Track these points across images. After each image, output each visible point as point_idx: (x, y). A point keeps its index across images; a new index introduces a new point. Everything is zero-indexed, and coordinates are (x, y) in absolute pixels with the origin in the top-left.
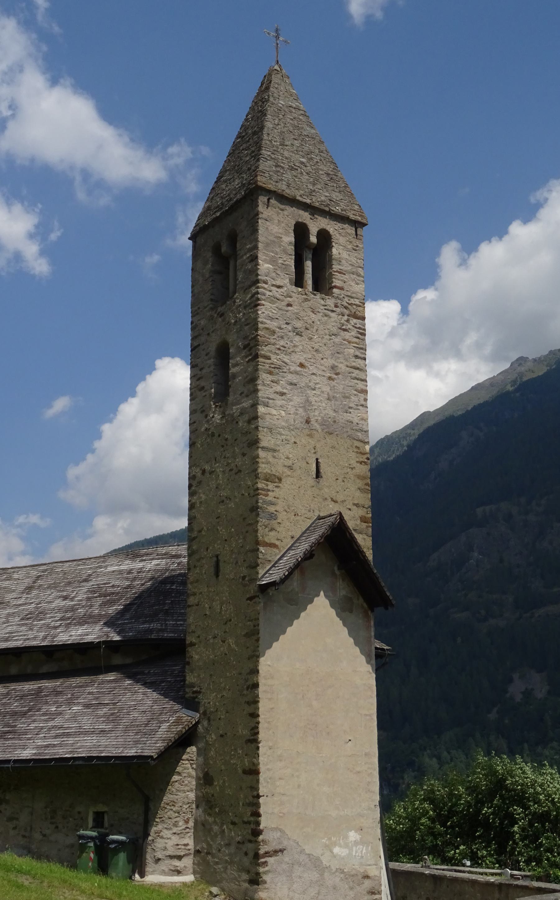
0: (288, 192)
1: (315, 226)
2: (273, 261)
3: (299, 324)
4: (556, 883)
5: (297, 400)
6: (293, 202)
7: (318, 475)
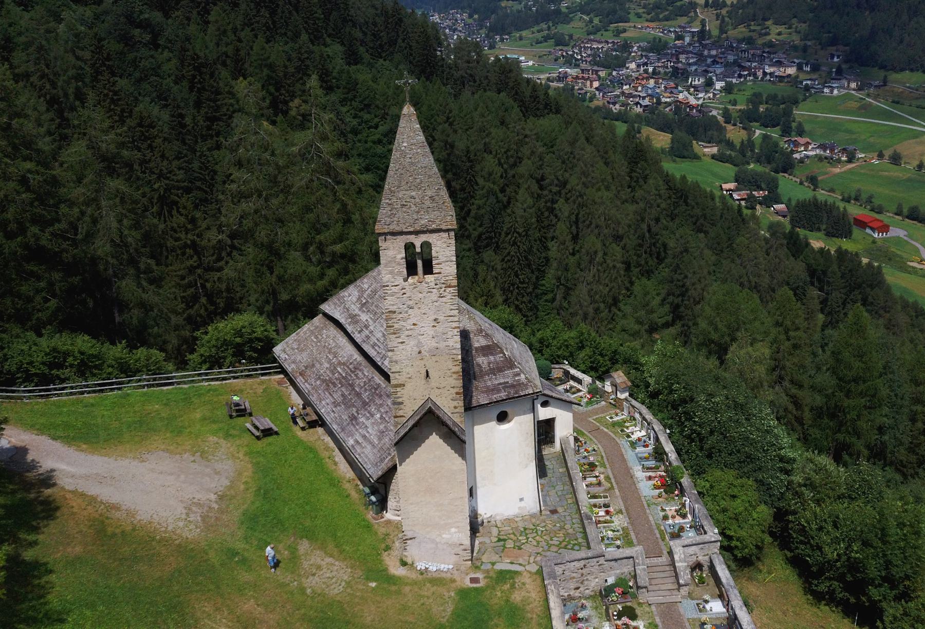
0: (398, 229)
1: (418, 241)
2: (391, 273)
3: (411, 303)
4: (912, 70)
5: (413, 343)
6: (401, 233)
7: (428, 376)
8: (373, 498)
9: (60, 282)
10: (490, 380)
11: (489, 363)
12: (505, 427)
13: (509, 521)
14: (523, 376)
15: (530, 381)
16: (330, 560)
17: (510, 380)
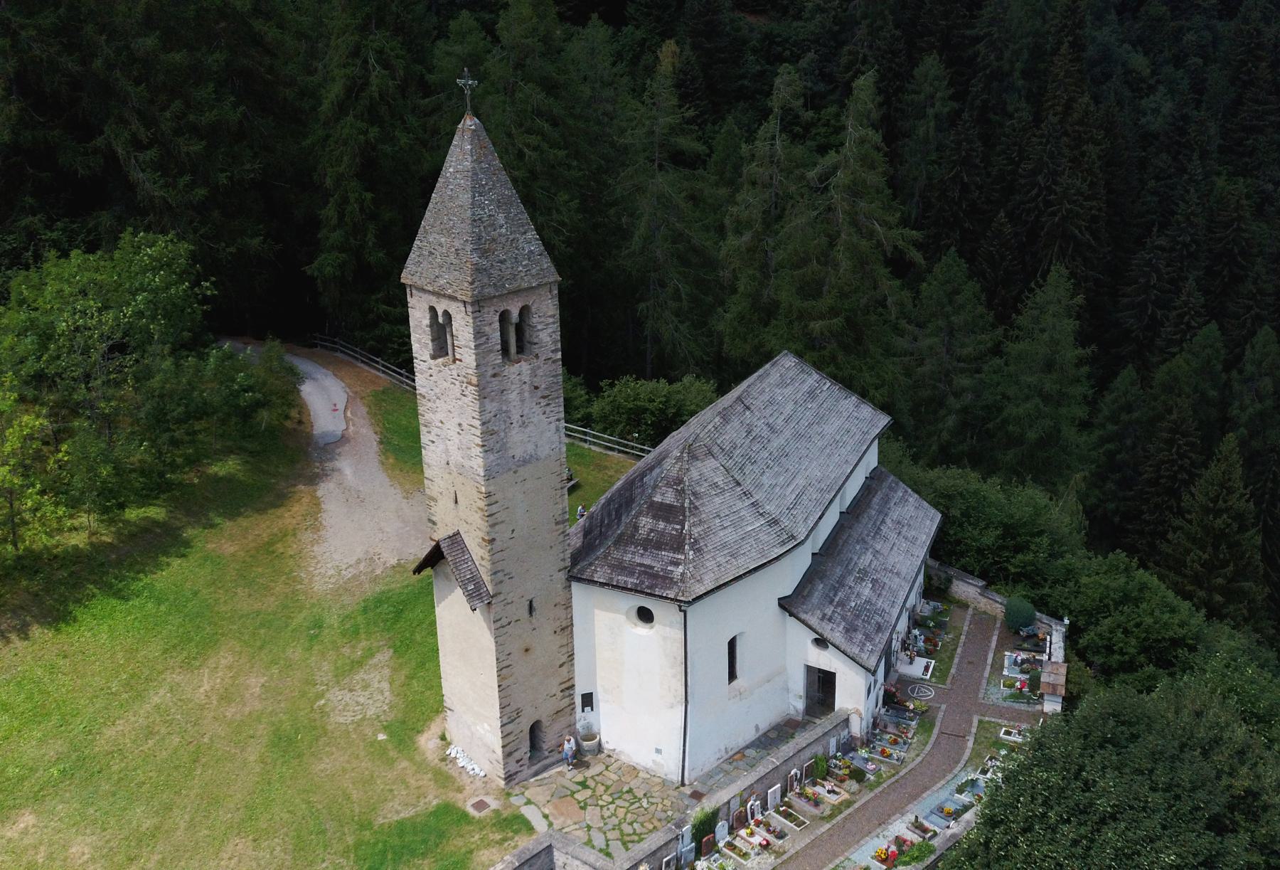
8: (105, 471)
9: (111, 443)
10: (633, 553)
11: (652, 531)
12: (642, 630)
13: (634, 770)
14: (681, 569)
15: (682, 581)
16: (385, 685)
17: (658, 566)
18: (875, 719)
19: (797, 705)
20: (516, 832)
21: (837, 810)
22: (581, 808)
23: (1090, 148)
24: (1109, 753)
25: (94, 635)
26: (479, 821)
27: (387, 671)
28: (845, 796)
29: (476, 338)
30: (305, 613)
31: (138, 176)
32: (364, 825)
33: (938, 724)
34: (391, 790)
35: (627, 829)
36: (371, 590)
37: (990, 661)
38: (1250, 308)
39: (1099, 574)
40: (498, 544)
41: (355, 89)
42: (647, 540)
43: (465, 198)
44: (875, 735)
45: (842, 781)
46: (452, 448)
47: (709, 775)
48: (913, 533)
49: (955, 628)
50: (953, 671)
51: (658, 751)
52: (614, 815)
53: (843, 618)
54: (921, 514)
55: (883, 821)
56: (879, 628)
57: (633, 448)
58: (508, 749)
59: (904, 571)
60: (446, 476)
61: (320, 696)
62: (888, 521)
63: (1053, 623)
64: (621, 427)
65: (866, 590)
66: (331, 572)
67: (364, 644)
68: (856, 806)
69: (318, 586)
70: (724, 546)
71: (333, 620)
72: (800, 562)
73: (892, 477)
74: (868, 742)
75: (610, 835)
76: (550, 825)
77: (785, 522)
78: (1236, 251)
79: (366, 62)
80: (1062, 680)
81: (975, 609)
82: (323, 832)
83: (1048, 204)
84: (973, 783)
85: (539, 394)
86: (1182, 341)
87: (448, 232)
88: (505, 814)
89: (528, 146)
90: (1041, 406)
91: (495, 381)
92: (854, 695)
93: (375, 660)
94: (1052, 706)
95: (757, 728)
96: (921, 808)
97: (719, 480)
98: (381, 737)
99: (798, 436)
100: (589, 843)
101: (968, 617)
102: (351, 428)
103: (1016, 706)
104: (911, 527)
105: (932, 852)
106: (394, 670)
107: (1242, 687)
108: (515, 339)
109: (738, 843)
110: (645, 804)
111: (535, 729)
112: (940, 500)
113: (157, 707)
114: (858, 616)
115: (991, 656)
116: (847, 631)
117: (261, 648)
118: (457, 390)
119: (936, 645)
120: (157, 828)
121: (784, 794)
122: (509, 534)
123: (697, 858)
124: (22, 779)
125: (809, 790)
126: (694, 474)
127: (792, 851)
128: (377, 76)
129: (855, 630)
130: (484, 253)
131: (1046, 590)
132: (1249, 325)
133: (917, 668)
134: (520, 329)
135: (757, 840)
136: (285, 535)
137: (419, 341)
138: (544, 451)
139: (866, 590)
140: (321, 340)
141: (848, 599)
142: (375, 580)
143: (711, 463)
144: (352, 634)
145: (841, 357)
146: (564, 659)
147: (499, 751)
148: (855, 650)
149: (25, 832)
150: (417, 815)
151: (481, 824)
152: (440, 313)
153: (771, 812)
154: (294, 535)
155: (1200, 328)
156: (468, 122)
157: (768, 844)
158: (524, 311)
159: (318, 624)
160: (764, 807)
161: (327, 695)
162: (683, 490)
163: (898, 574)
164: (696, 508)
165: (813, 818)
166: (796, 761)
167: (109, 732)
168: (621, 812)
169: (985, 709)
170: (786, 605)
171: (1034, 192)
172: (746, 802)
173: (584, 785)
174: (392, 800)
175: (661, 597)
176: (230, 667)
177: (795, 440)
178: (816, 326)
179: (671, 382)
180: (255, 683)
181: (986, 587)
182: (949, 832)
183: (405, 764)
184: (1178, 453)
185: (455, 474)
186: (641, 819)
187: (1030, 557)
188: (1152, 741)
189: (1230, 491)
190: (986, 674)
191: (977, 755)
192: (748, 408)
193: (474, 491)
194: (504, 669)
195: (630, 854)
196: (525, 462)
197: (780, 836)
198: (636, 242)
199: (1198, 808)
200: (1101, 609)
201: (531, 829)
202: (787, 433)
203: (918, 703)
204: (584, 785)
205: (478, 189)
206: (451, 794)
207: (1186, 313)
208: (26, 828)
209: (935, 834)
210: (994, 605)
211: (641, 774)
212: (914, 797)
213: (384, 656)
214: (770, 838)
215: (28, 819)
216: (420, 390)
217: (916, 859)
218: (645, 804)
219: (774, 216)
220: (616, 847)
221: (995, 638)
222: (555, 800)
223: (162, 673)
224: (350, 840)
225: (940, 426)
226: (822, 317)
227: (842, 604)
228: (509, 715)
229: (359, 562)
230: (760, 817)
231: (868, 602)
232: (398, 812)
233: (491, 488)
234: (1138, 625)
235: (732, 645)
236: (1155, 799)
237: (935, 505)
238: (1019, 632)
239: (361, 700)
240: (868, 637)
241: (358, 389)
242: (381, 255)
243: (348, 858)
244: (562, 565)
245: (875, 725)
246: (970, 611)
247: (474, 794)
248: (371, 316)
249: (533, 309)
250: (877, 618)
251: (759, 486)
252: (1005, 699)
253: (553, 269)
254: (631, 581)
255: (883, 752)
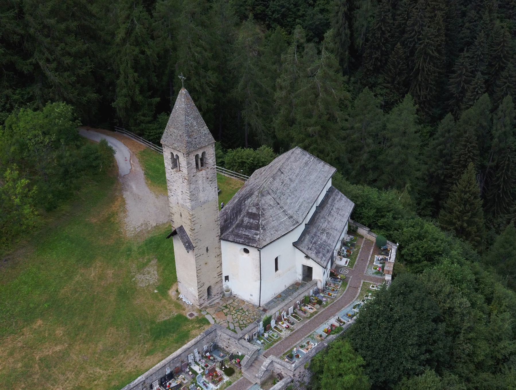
11: (248, 222)
12: (245, 255)
13: (243, 301)
14: (258, 236)
15: (259, 241)
16: (156, 272)
18: (326, 282)
19: (299, 277)
20: (204, 324)
21: (312, 315)
22: (226, 315)
23: (439, 13)
24: (401, 298)
25: (51, 255)
26: (191, 320)
27: (156, 267)
28: (315, 310)
29: (187, 165)
30: (125, 245)
31: (48, 73)
32: (152, 322)
33: (349, 283)
34: (161, 310)
35: (241, 322)
36: (147, 236)
37: (369, 259)
38: (505, 83)
39: (411, 224)
40: (196, 231)
41: (129, 32)
42: (246, 226)
43: (183, 118)
44: (326, 288)
45: (314, 305)
46: (180, 198)
47: (269, 303)
48: (343, 212)
49: (358, 246)
50: (356, 263)
51: (251, 295)
52: (237, 317)
53: (315, 248)
54: (347, 204)
55: (327, 319)
56: (328, 251)
57: (240, 176)
58: (200, 296)
59: (338, 228)
60: (177, 207)
61: (133, 277)
62: (334, 208)
63: (393, 244)
64: (236, 168)
65: (324, 237)
66: (132, 229)
67: (147, 257)
68: (319, 313)
69: (128, 235)
70: (273, 227)
71: (135, 248)
72: (302, 228)
73: (337, 190)
74: (323, 291)
75: (236, 325)
76: (215, 321)
77: (295, 217)
78: (502, 56)
79: (132, 20)
80: (392, 269)
81: (366, 238)
82: (139, 325)
83: (419, 39)
84: (359, 305)
85: (209, 180)
86: (474, 99)
87: (177, 128)
88: (200, 318)
89: (197, 52)
90: (400, 150)
91: (194, 178)
92: (320, 275)
93: (151, 263)
94: (388, 277)
95: (285, 286)
96: (340, 315)
97: (272, 203)
98: (156, 291)
99: (301, 182)
100: (228, 328)
101: (363, 242)
102: (133, 168)
103: (377, 276)
104: (344, 207)
105: (342, 330)
106: (158, 267)
107: (453, 270)
108: (201, 162)
109: (278, 326)
110: (247, 314)
111: (209, 289)
112: (353, 198)
113: (77, 282)
114: (321, 247)
115: (370, 257)
116: (316, 253)
117: (110, 259)
118: (181, 180)
119: (350, 253)
120: (83, 324)
121: (294, 309)
122: (199, 227)
123: (265, 332)
124: (36, 308)
125: (303, 308)
126: (263, 202)
127: (296, 329)
128: (138, 27)
129: (319, 253)
130: (189, 136)
131: (391, 232)
132: (504, 90)
133: (343, 262)
134: (202, 160)
135: (285, 325)
136: (114, 215)
137: (167, 163)
138: (210, 199)
139: (324, 237)
140: (118, 129)
141: (318, 241)
142: (148, 232)
143: (269, 197)
144: (142, 253)
145: (319, 141)
146: (219, 265)
147: (197, 297)
148: (319, 260)
149: (40, 326)
150: (170, 319)
151: (192, 321)
152: (175, 155)
153: (290, 315)
154: (117, 214)
155: (482, 94)
156: (183, 91)
157: (289, 327)
158: (204, 154)
159: (130, 250)
160: (287, 314)
161: (136, 277)
162: (259, 208)
163: (336, 230)
164: (264, 214)
165: (304, 318)
166: (298, 298)
167: (62, 291)
168: (239, 317)
169: (365, 278)
170: (295, 245)
171: (413, 34)
172: (281, 313)
173: (226, 307)
174: (161, 314)
175: (252, 246)
176: (100, 267)
177: (301, 178)
178: (310, 129)
179: (255, 149)
180: (110, 272)
181: (370, 231)
182: (349, 323)
183: (165, 301)
184: (468, 150)
185: (180, 207)
186: (246, 319)
187: (385, 220)
188: (416, 293)
189: (470, 184)
190: (368, 264)
191: (361, 294)
192: (282, 173)
193: (187, 213)
194: (198, 270)
195: (242, 332)
196: (204, 203)
197: (293, 324)
198: (240, 86)
199: (429, 316)
200: (410, 240)
201: (209, 323)
202: (297, 181)
203: (342, 275)
204: (226, 307)
205: (187, 115)
206: (181, 311)
207: (476, 87)
208: (40, 325)
209: (344, 323)
210: (372, 237)
211: (246, 303)
212: (338, 310)
213: (154, 262)
214: (289, 324)
215: (40, 322)
216: (168, 178)
217: (337, 332)
218: (247, 314)
219: (293, 87)
220: (238, 329)
221: (372, 250)
222: (216, 313)
223: (77, 269)
224: (148, 327)
225: (361, 158)
226: (312, 125)
227: (315, 243)
228: (200, 285)
229: (142, 225)
230: (285, 317)
231: (325, 241)
232: (164, 318)
233: (193, 213)
234: (422, 247)
235: (276, 260)
236: (414, 313)
237: (352, 200)
238: (381, 248)
239: (148, 278)
240: (324, 255)
241: (134, 151)
242: (140, 98)
243: (148, 333)
244: (218, 235)
245: (326, 284)
246: (364, 239)
247: (189, 311)
248: (138, 121)
249: (206, 153)
250: (328, 247)
251: (286, 204)
252: (373, 274)
253: (213, 138)
254: (241, 240)
255: (329, 294)
